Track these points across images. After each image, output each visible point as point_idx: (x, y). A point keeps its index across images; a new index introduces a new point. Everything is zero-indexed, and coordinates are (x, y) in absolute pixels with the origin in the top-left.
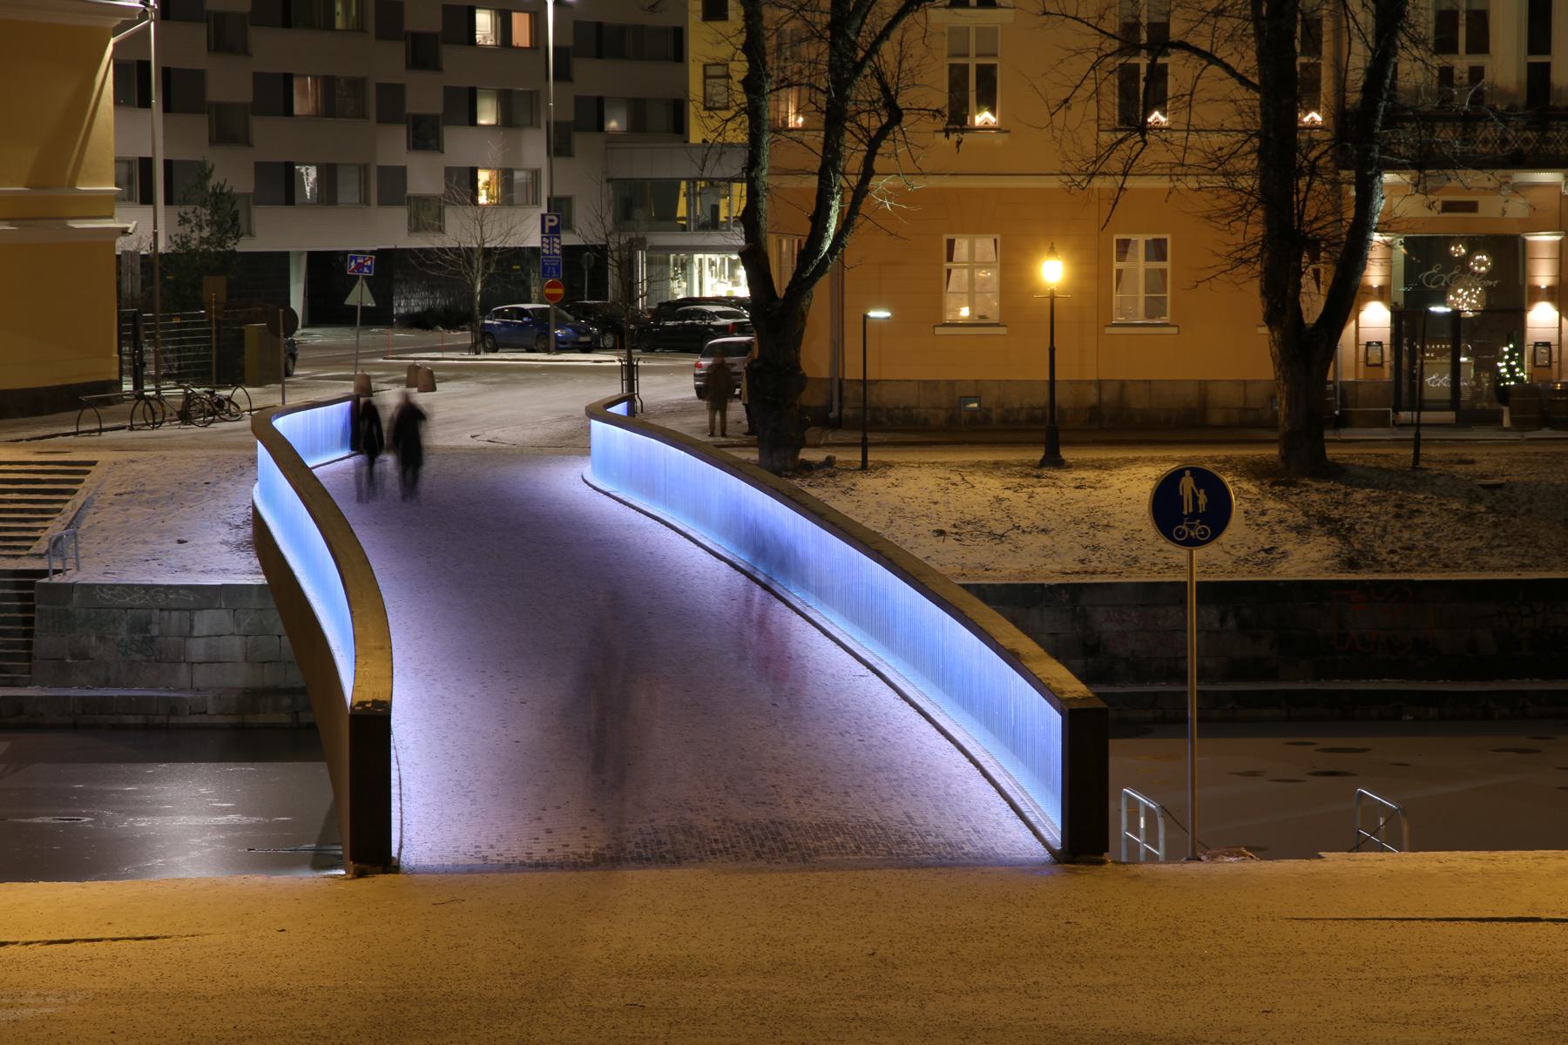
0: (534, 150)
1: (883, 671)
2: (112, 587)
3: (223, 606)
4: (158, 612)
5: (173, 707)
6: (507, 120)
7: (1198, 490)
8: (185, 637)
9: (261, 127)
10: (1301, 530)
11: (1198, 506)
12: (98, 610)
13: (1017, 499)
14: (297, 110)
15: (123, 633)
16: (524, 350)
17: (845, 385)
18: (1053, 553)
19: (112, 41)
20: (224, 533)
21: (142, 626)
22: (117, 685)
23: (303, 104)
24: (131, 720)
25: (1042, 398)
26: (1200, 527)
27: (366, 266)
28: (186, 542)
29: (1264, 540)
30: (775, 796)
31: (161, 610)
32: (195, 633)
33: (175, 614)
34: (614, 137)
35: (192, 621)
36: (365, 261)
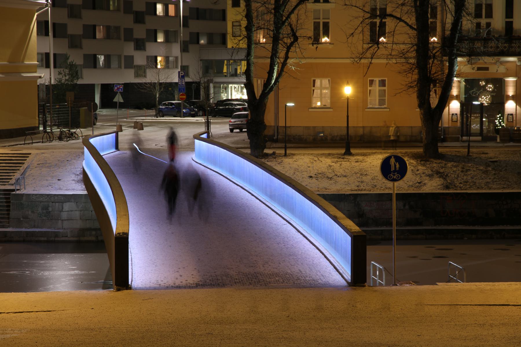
0: (176, 50)
4: (51, 203)
5: (56, 234)
6: (167, 40)
8: (60, 212)
10: (430, 176)
11: (396, 168)
13: (336, 166)
15: (40, 210)
18: (348, 184)
19: (36, 14)
20: (73, 177)
21: (46, 208)
22: (38, 227)
23: (99, 35)
24: (42, 239)
25: (344, 132)
26: (397, 175)
29: (418, 179)
30: (256, 264)
31: (52, 202)
32: (64, 210)
33: (57, 204)
34: (203, 46)
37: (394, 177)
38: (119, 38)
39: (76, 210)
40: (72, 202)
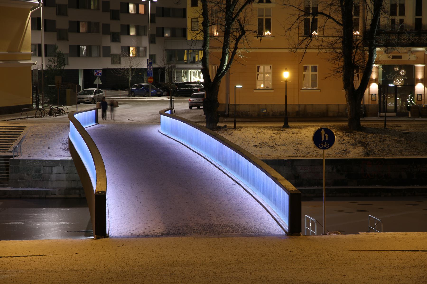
0: (145, 42)
1: (240, 183)
2: (30, 160)
3: (61, 166)
4: (43, 167)
5: (47, 193)
6: (138, 34)
7: (326, 134)
8: (50, 174)
9: (71, 35)
10: (354, 145)
12: (26, 167)
13: (277, 137)
14: (81, 31)
15: (33, 173)
16: (142, 96)
17: (230, 105)
18: (286, 151)
19: (30, 12)
20: (61, 146)
21: (38, 171)
24: (36, 196)
25: (283, 109)
26: (326, 144)
27: (100, 73)
28: (50, 148)
29: (344, 148)
31: (44, 166)
32: (53, 173)
33: (47, 168)
34: (167, 38)
35: (52, 170)
36: (99, 72)
37: (324, 146)
38: (98, 32)
39: (63, 173)
40: (60, 166)
